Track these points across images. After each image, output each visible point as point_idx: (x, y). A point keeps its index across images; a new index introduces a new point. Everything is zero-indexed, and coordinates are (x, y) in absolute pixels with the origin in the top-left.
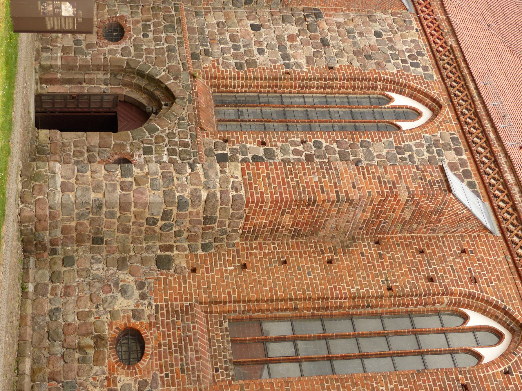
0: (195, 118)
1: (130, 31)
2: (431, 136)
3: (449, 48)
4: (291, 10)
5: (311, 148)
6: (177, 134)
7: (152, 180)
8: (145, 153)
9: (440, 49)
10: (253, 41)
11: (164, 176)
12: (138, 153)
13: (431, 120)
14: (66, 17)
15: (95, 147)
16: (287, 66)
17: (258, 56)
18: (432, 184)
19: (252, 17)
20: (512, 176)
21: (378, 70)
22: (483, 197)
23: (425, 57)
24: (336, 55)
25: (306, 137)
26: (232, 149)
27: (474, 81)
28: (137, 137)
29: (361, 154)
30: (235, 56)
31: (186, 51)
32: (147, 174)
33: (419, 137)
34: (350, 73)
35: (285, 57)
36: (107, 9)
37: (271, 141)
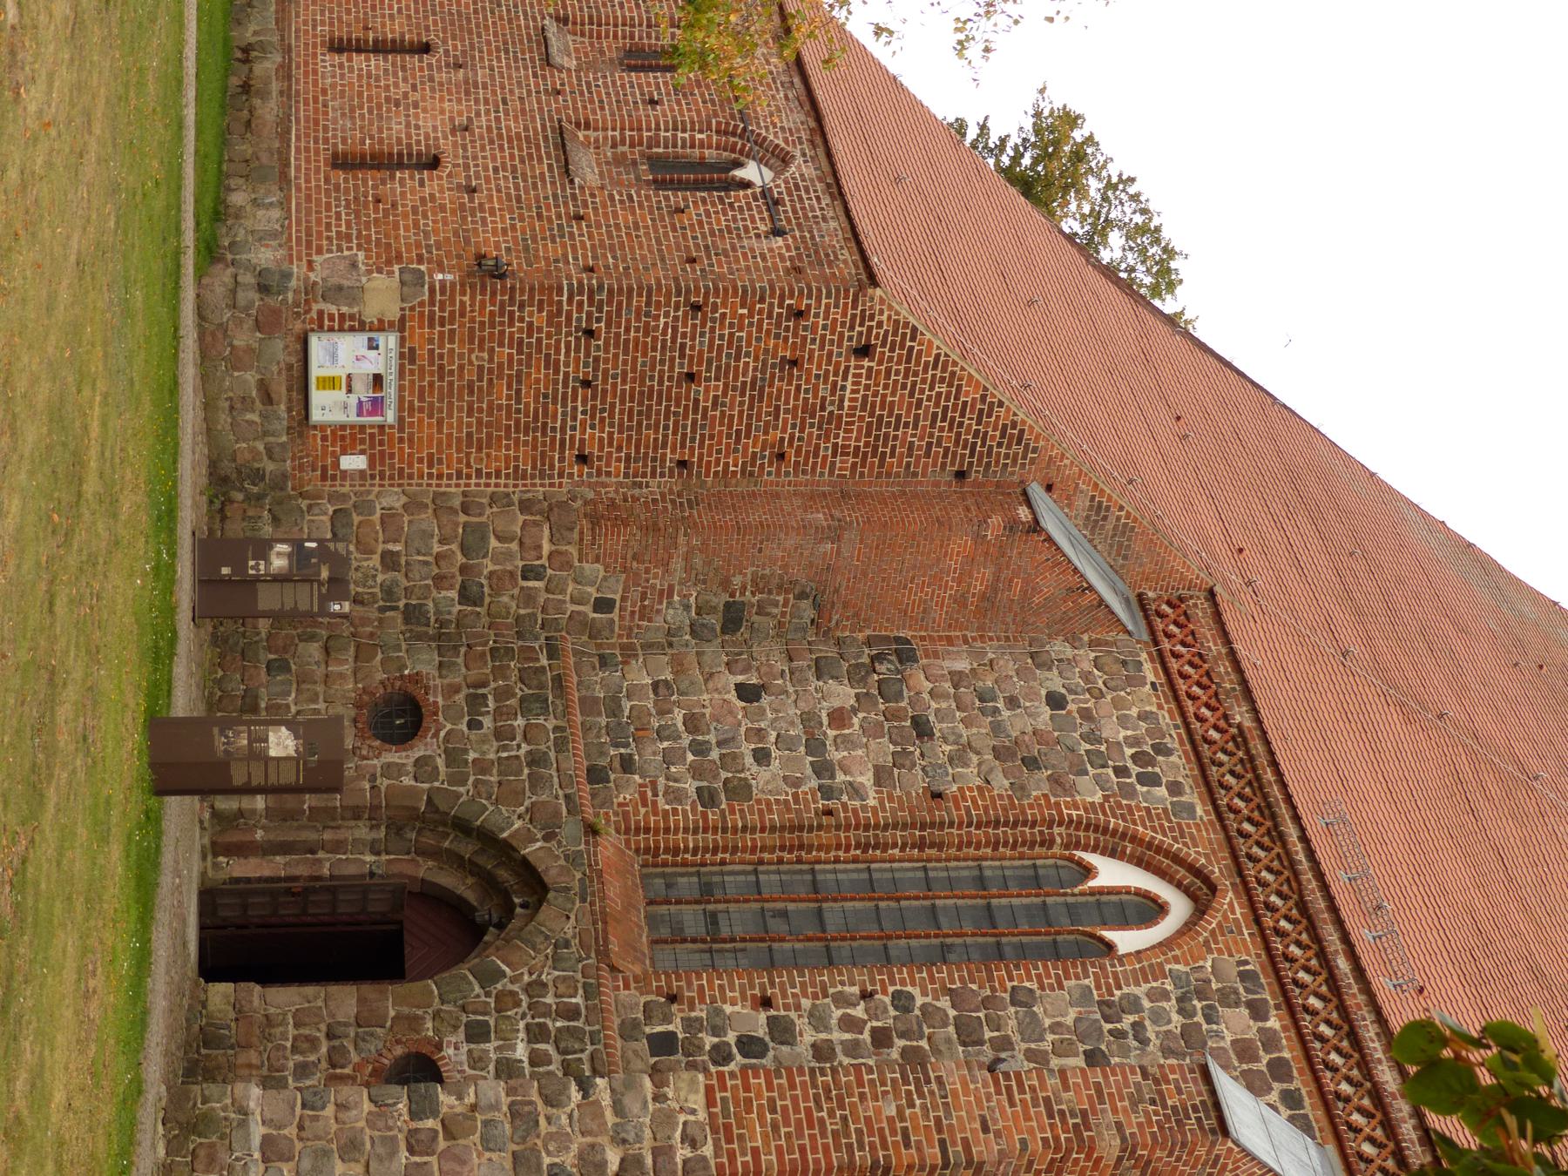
0: (597, 939)
1: (436, 714)
2: (1187, 969)
3: (1234, 731)
4: (839, 642)
5: (885, 1010)
6: (551, 984)
7: (486, 1123)
8: (470, 1039)
9: (1214, 734)
10: (743, 730)
11: (514, 1113)
12: (453, 1040)
13: (1188, 927)
14: (278, 759)
15: (346, 1025)
16: (827, 792)
17: (755, 768)
18: (1180, 1114)
19: (740, 666)
20: (1396, 1074)
21: (1055, 795)
22: (1321, 1130)
23: (1173, 758)
24: (951, 760)
25: (873, 982)
26: (689, 1019)
27: (1297, 818)
28: (452, 996)
29: (1012, 1023)
30: (696, 771)
31: (577, 763)
32: (474, 1108)
33: (1158, 972)
34: (986, 808)
35: (823, 769)
36: (379, 656)
37: (784, 996)
